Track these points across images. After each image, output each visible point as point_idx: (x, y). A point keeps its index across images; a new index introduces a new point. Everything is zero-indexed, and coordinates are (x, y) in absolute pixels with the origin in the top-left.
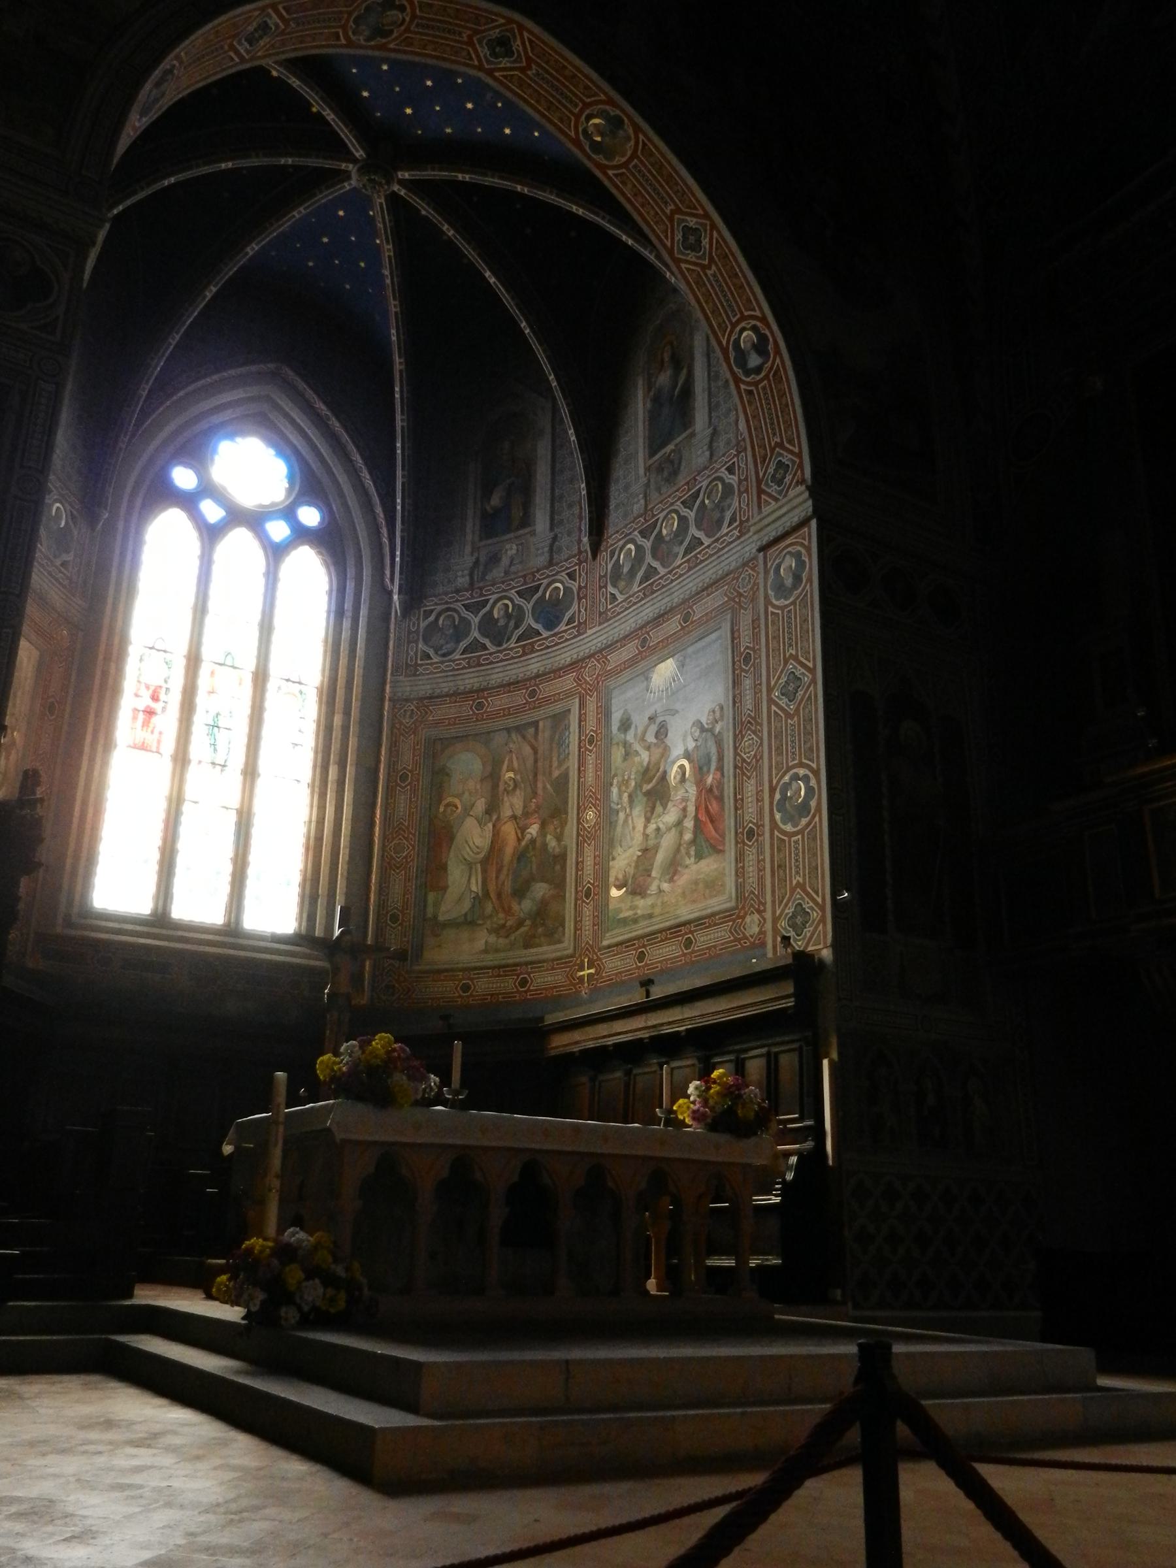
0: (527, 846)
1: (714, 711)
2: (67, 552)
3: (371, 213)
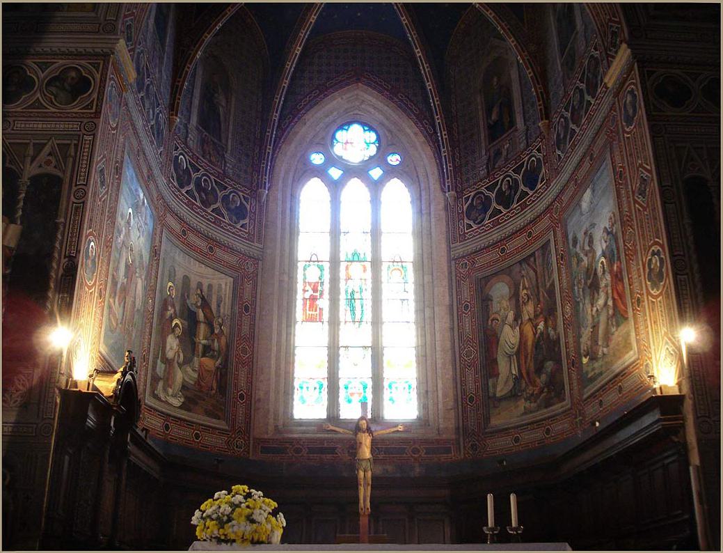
0: (539, 337)
1: (611, 218)
2: (244, 218)
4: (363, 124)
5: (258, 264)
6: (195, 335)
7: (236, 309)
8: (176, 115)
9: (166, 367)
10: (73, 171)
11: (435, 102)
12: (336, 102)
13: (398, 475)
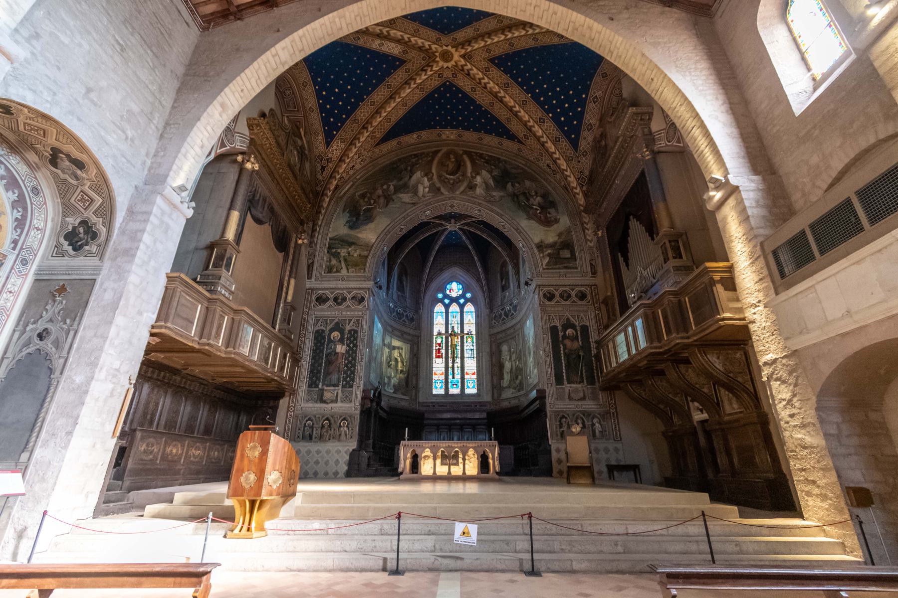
3: (550, 115)
4: (457, 282)
11: (482, 276)
12: (446, 274)
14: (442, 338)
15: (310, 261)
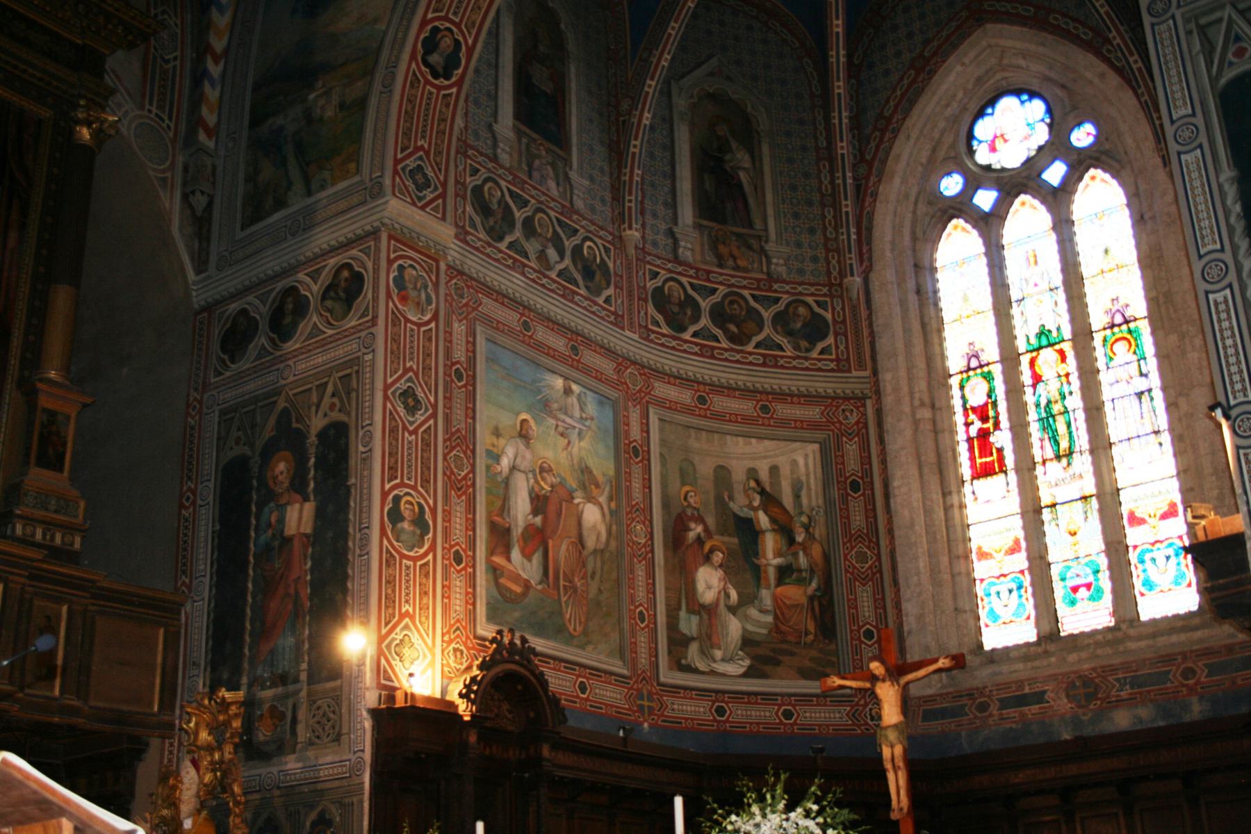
2: (824, 336)
4: (1017, 92)
5: (864, 406)
6: (756, 554)
7: (835, 493)
8: (630, 228)
9: (701, 618)
10: (357, 409)
13: (1162, 723)
14: (988, 377)
15: (200, 201)
